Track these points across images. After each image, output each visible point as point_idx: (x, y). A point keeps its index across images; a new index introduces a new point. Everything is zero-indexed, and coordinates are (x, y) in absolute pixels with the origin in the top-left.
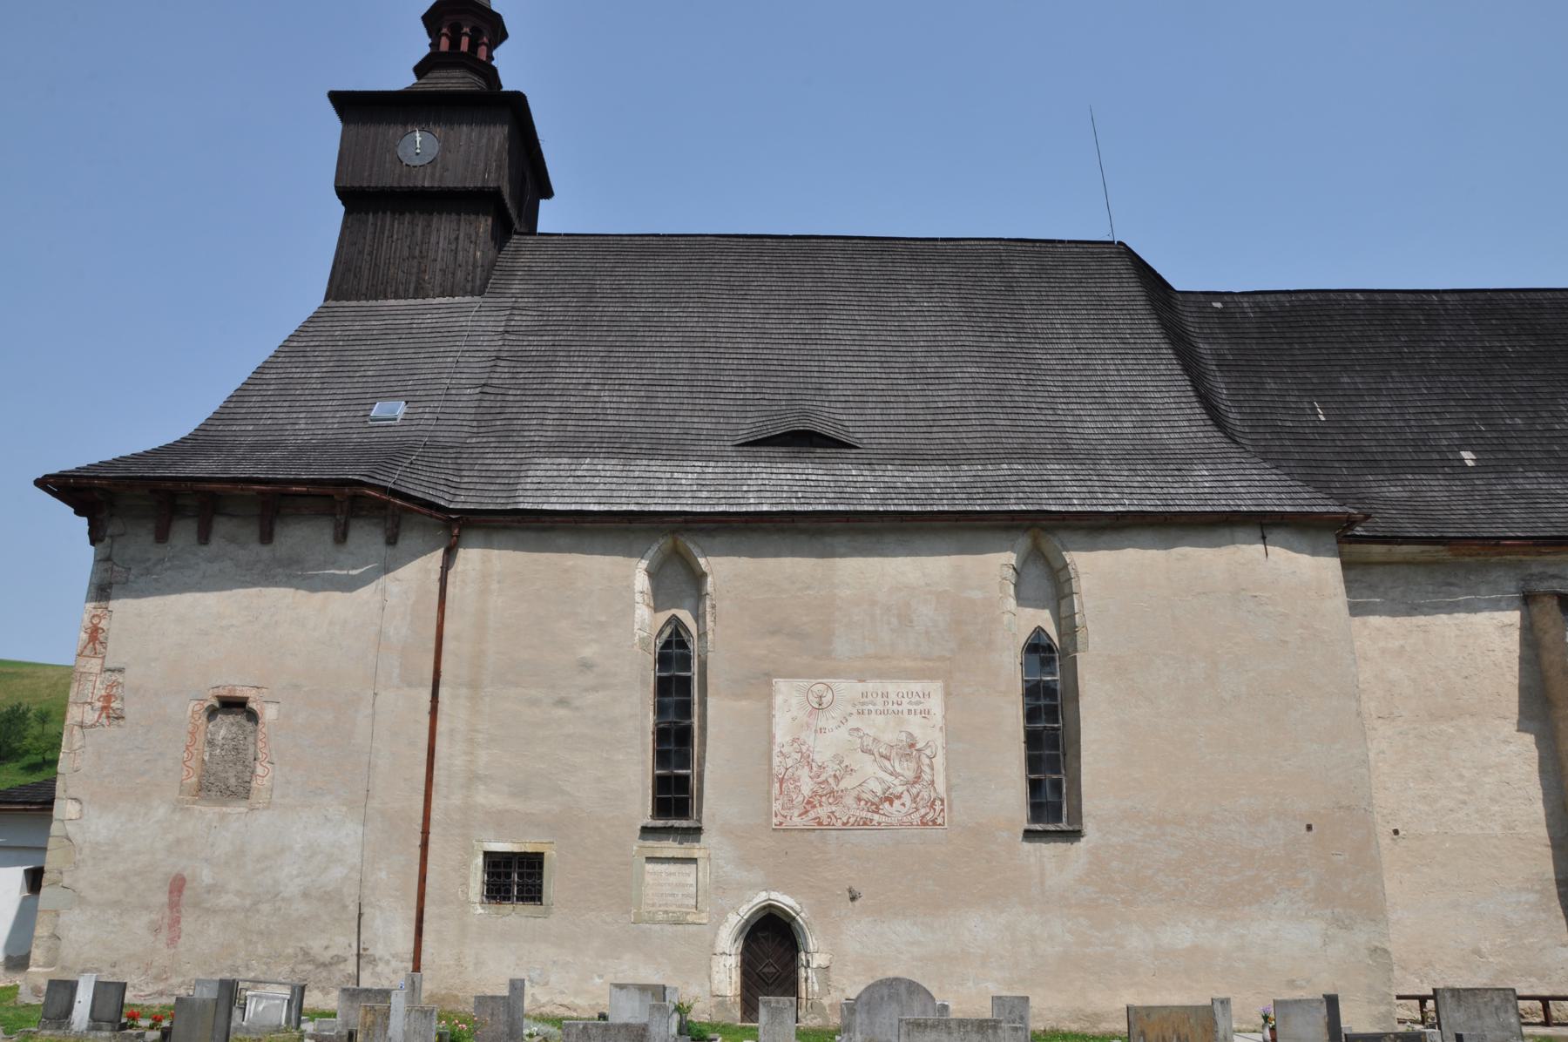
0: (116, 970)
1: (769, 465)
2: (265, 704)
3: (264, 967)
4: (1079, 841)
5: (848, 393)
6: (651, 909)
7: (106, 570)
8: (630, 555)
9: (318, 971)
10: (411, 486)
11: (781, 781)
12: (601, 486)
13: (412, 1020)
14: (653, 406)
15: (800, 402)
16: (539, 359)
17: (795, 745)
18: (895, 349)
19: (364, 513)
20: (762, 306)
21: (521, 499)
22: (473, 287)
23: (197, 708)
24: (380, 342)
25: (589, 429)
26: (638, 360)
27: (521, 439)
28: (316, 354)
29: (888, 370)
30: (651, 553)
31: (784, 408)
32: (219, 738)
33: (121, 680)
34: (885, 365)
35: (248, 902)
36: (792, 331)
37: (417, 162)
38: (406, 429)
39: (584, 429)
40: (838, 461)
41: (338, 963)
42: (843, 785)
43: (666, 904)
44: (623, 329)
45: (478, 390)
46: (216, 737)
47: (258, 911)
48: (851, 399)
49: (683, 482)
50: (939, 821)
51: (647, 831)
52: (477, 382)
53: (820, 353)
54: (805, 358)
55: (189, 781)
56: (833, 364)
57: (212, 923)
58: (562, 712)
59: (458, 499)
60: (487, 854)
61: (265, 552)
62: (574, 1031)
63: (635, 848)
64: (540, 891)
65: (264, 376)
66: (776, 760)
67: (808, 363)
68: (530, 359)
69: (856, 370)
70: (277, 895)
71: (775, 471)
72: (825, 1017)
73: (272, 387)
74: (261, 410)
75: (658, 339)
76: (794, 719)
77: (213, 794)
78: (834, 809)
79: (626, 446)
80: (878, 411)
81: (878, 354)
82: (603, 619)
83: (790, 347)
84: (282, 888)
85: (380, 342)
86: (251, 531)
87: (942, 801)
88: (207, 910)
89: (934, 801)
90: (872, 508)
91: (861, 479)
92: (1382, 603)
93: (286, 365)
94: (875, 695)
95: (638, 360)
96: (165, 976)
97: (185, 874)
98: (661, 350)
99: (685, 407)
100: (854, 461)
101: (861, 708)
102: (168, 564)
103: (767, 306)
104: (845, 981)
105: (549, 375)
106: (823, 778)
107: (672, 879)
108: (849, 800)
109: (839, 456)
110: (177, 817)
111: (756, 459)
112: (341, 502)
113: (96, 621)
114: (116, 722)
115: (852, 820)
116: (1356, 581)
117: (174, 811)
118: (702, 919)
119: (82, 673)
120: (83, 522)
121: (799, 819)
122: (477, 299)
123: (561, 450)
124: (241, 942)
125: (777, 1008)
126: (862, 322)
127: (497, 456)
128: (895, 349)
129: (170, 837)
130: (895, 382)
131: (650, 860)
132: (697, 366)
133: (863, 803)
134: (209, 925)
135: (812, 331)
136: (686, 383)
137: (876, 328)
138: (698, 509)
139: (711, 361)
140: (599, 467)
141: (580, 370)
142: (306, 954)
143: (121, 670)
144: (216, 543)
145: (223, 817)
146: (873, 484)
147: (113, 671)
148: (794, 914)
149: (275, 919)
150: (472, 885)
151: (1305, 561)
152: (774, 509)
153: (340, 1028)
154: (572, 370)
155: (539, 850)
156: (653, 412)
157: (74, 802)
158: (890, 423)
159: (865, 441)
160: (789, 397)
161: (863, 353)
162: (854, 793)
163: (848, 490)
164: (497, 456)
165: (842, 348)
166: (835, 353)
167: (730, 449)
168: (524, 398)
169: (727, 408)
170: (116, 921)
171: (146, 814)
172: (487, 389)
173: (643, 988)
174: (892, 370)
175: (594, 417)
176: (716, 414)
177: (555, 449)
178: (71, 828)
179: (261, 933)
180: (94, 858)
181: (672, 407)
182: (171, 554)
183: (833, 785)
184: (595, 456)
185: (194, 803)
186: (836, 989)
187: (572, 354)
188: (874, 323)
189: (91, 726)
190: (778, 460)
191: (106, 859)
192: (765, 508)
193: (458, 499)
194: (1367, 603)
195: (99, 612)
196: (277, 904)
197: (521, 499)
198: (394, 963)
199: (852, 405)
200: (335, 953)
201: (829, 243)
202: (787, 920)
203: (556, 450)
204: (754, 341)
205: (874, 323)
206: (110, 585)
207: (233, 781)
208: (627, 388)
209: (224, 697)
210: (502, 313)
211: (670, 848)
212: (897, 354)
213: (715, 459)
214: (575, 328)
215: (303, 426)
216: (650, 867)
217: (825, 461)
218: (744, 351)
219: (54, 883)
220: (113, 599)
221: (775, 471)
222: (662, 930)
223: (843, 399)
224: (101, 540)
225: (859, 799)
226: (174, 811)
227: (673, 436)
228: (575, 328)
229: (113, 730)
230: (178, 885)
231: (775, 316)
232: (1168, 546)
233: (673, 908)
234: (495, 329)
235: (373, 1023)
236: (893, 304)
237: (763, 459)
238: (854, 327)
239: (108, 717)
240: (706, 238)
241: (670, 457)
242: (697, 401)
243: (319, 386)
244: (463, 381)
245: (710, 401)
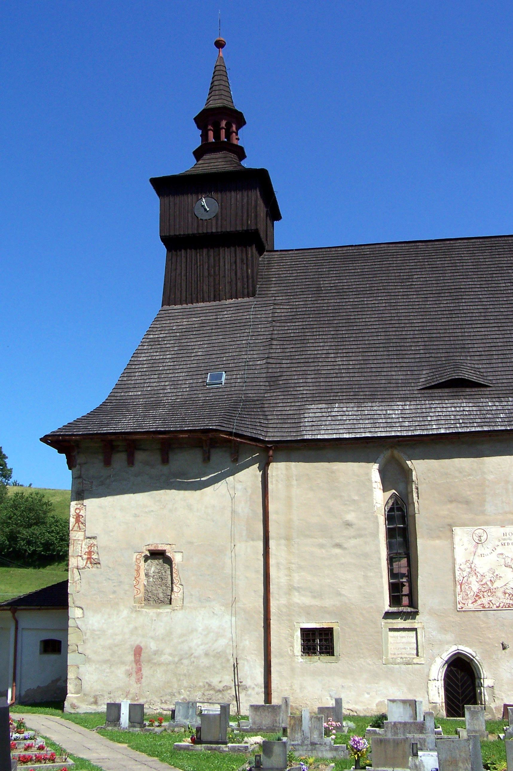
0: (111, 695)
1: (440, 402)
2: (175, 553)
3: (188, 693)
5: (481, 349)
6: (393, 656)
7: (79, 483)
8: (368, 461)
9: (217, 694)
10: (243, 429)
11: (461, 585)
12: (348, 422)
13: (313, 722)
14: (368, 366)
15: (453, 358)
16: (296, 338)
17: (468, 564)
18: (506, 317)
19: (218, 445)
20: (422, 293)
21: (304, 432)
22: (248, 292)
23: (138, 557)
24: (201, 332)
25: (334, 384)
26: (354, 335)
27: (296, 393)
28: (165, 342)
29: (503, 332)
30: (379, 459)
31: (444, 362)
33: (95, 543)
34: (501, 329)
35: (176, 659)
36: (443, 309)
37: (207, 217)
38: (229, 389)
39: (330, 384)
40: (480, 396)
41: (227, 689)
42: (495, 585)
43: (401, 654)
44: (342, 314)
45: (264, 361)
46: (149, 571)
47: (182, 664)
48: (483, 353)
49: (394, 416)
51: (388, 615)
52: (261, 356)
53: (461, 323)
54: (452, 327)
55: (138, 596)
56: (470, 330)
57: (158, 671)
58: (338, 551)
59: (269, 434)
60: (302, 629)
61: (165, 469)
62: (390, 725)
63: (383, 624)
64: (333, 648)
65: (139, 359)
66: (457, 573)
67: (455, 331)
68: (291, 339)
69: (484, 333)
70: (192, 654)
71: (444, 405)
72: (493, 714)
73: (145, 366)
74: (142, 381)
75: (364, 320)
76: (466, 550)
78: (491, 598)
79: (357, 394)
80: (500, 361)
81: (496, 321)
82: (356, 498)
83: (443, 320)
84: (193, 651)
85: (201, 332)
86: (157, 457)
88: (155, 664)
90: (503, 428)
91: (494, 408)
93: (150, 351)
94: (511, 534)
95: (354, 335)
96: (137, 699)
97: (142, 645)
98: (366, 327)
99: (386, 365)
100: (489, 396)
101: (503, 542)
102: (113, 479)
103: (425, 292)
104: (503, 694)
105: (304, 349)
106: (484, 582)
107: (404, 640)
108: (500, 594)
109: (480, 393)
110: (134, 615)
111: (432, 398)
112: (205, 440)
113: (78, 511)
115: (502, 605)
118: (421, 661)
120: (64, 456)
121: (472, 605)
122: (251, 299)
123: (320, 399)
124: (175, 680)
125: (474, 711)
126: (484, 300)
127: (285, 405)
128: (506, 317)
129: (131, 626)
130: (508, 340)
131: (391, 630)
132: (389, 337)
133: (507, 595)
134: (157, 672)
135: (455, 308)
136: (385, 349)
137: (493, 303)
138: (404, 434)
139: (397, 333)
140: (345, 409)
141: (321, 344)
142: (210, 685)
143: (94, 538)
144: (138, 467)
146: (502, 412)
148: (472, 658)
149: (191, 668)
150: (295, 646)
152: (448, 432)
153: (251, 725)
154: (317, 344)
156: (368, 370)
157: (78, 608)
158: (507, 369)
159: (494, 382)
160: (446, 355)
161: (487, 322)
162: (502, 590)
163: (488, 416)
164: (285, 405)
165: (474, 319)
166: (470, 322)
167: (416, 392)
168: (292, 365)
169: (411, 365)
170: (108, 670)
172: (270, 361)
173: (404, 702)
174: (505, 332)
175: (335, 375)
176: (405, 369)
177: (315, 399)
178: (79, 623)
179: (185, 675)
181: (379, 366)
183: (490, 585)
184: (340, 401)
186: (498, 698)
187: (315, 334)
188: (492, 299)
189: (83, 568)
190: (445, 398)
191: (99, 638)
192: (443, 431)
193: (269, 434)
195: (79, 506)
196: (193, 659)
197: (304, 432)
198: (257, 689)
199: (484, 357)
200: (225, 685)
201: (458, 244)
202: (468, 661)
203: (318, 399)
204: (421, 317)
205: (492, 299)
206: (83, 491)
207: (161, 595)
208: (351, 354)
209: (152, 550)
210: (268, 308)
211: (400, 623)
212: (507, 321)
213: (409, 399)
214: (314, 316)
215: (169, 391)
216: (391, 634)
217: (473, 397)
218: (416, 325)
219: (74, 651)
220: (85, 499)
221: (444, 405)
222: (400, 667)
223: (478, 354)
224: (75, 467)
225: (505, 593)
227: (382, 386)
228: (314, 316)
229: (94, 570)
230: (138, 651)
231: (431, 299)
233: (406, 656)
234: (266, 319)
235: (295, 724)
236: (502, 285)
237: (436, 398)
238: (479, 303)
239: (91, 563)
240: (382, 246)
241: (383, 400)
242: (393, 361)
243: (172, 364)
244: (255, 356)
245: (400, 361)
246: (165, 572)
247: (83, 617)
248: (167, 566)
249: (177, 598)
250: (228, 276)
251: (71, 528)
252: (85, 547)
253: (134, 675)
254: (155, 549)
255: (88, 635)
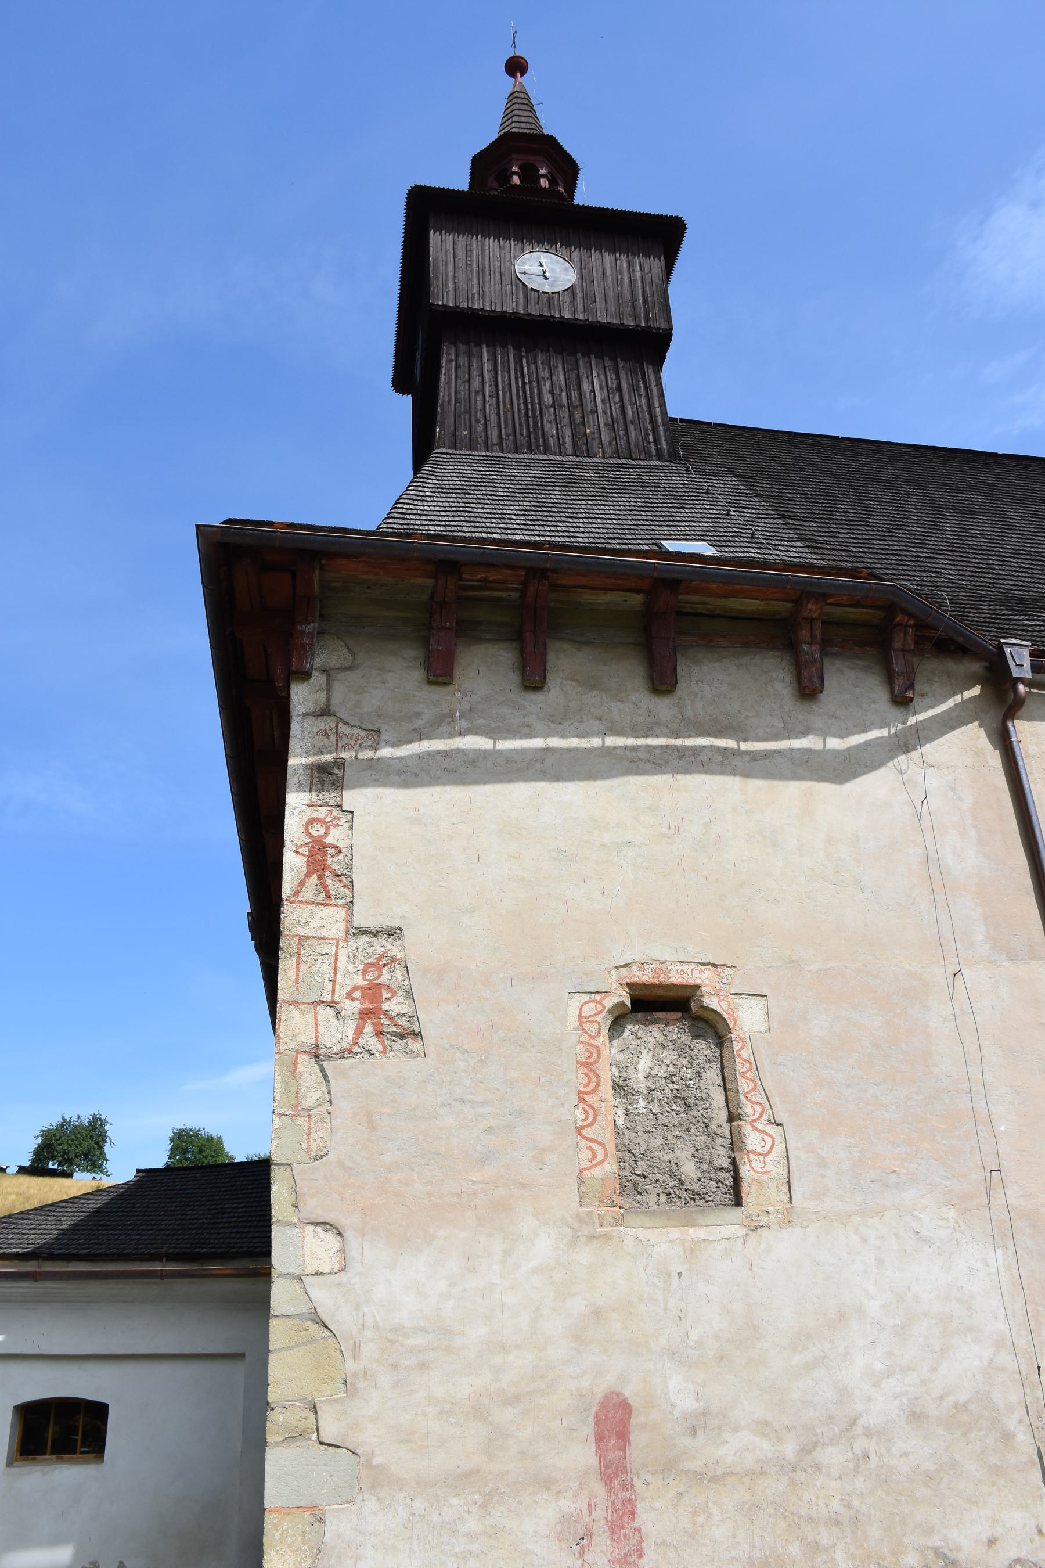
2: (736, 1000)
32: (639, 1080)
33: (396, 952)
35: (789, 1449)
47: (818, 1467)
55: (597, 1172)
57: (715, 1510)
61: (663, 707)
70: (853, 1423)
77: (652, 1199)
88: (697, 1476)
97: (627, 1392)
110: (584, 1256)
113: (317, 830)
114: (399, 1044)
117: (574, 1242)
119: (301, 938)
124: (795, 1549)
134: (709, 1516)
145: (693, 1250)
147: (375, 934)
157: (319, 1229)
170: (472, 1524)
171: (507, 1253)
178: (321, 1295)
180: (394, 1367)
182: (466, 706)
185: (619, 1222)
191: (423, 1366)
195: (322, 813)
200: (1013, 1554)
219: (297, 1436)
226: (574, 1242)
239: (380, 1034)
246: (698, 1075)
247: (343, 1269)
248: (703, 1049)
249: (765, 1177)
250: (604, 412)
251: (287, 889)
252: (351, 967)
253: (602, 1540)
254: (656, 981)
255: (370, 1350)
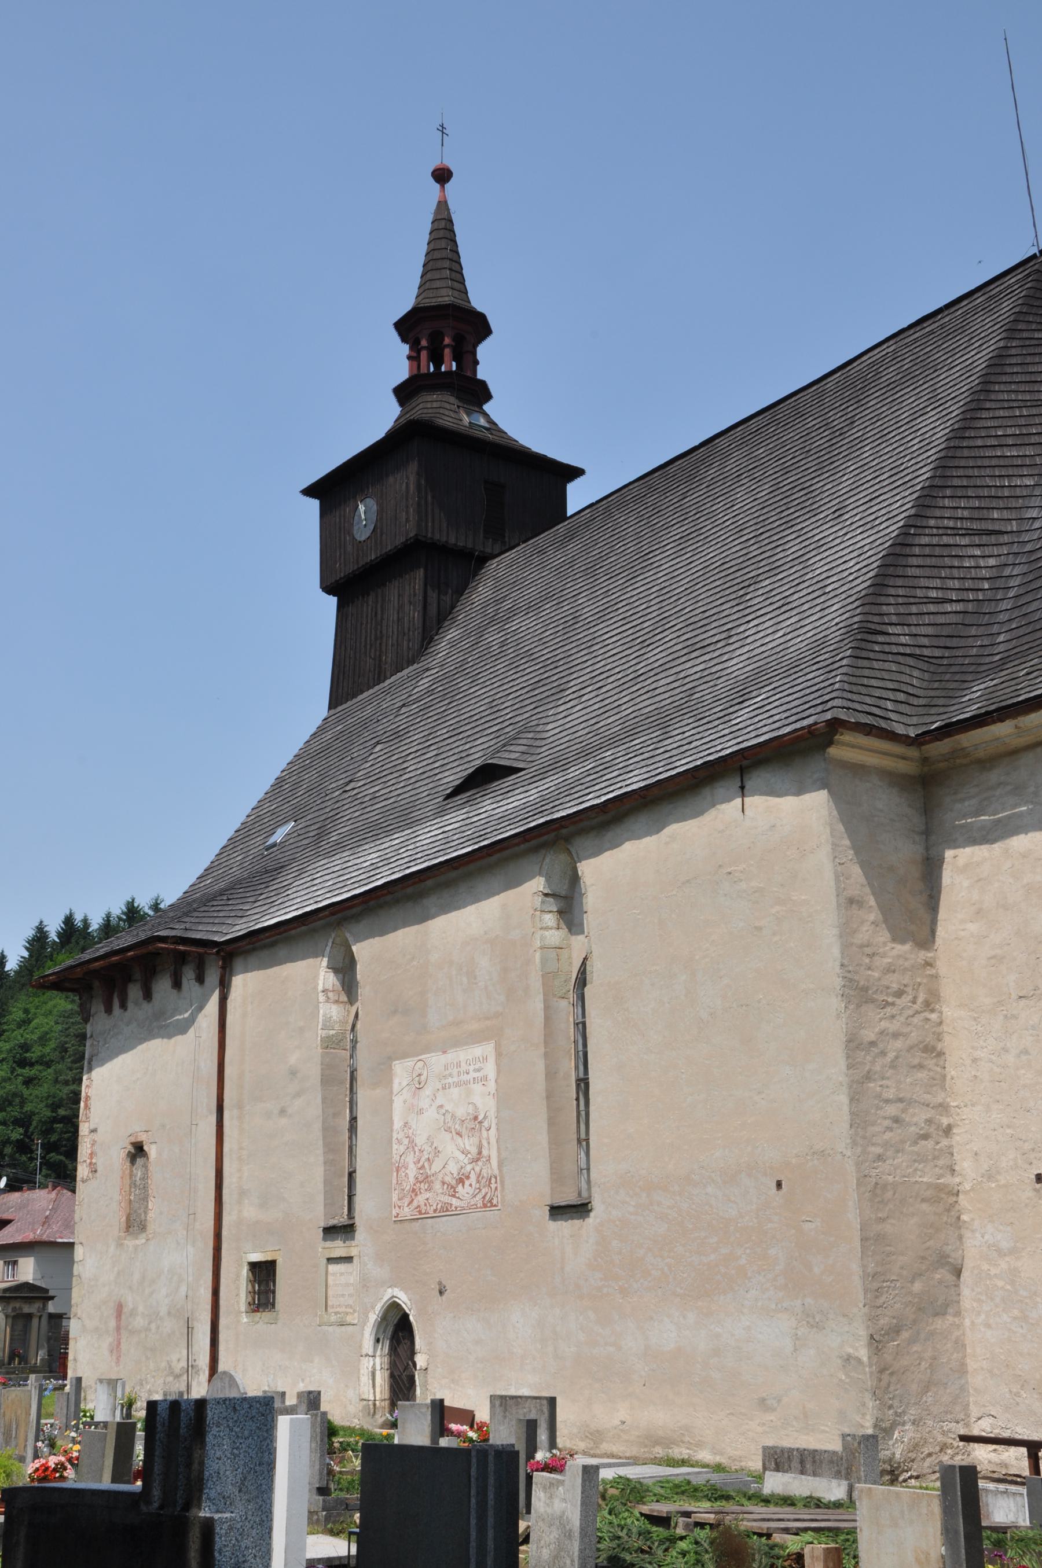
4: (588, 1216)
50: (495, 1202)
58: (284, 1121)
87: (496, 1178)
89: (490, 1179)
92: (1030, 812)
116: (1000, 784)
118: (353, 1319)
131: (330, 1260)
151: (788, 804)
155: (274, 1258)
194: (1009, 817)
216: (332, 1268)
230: (120, 1310)
232: (700, 813)
253: (115, 1351)
